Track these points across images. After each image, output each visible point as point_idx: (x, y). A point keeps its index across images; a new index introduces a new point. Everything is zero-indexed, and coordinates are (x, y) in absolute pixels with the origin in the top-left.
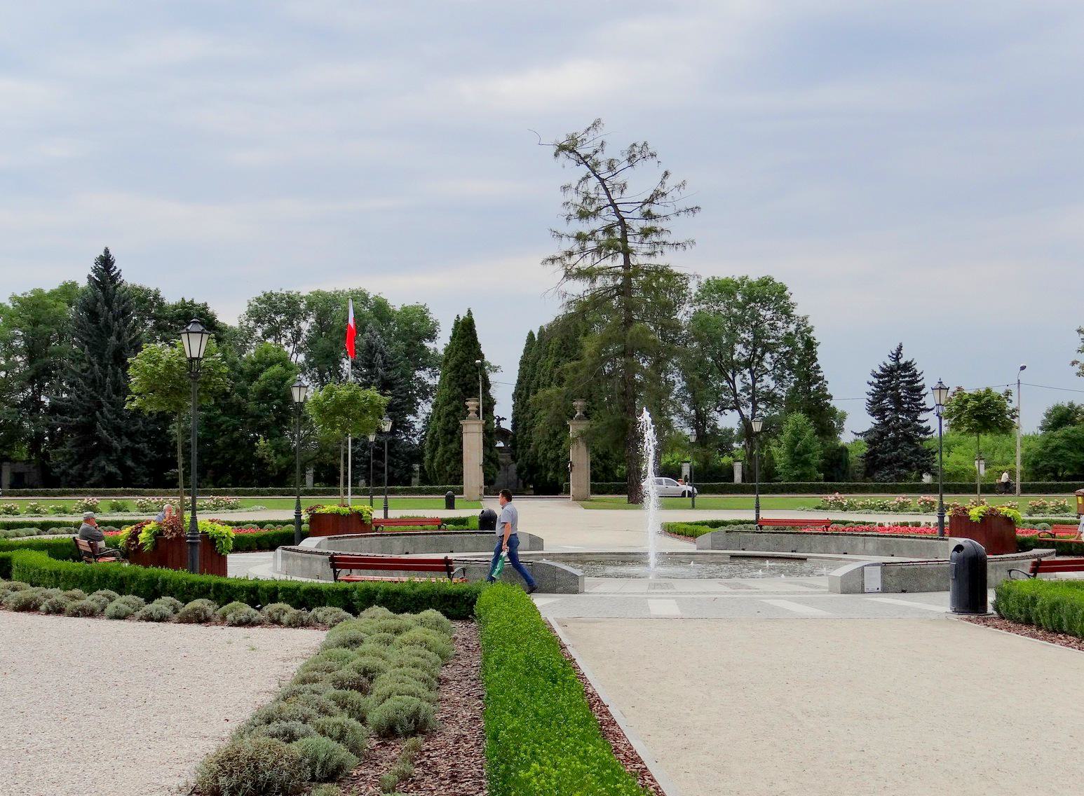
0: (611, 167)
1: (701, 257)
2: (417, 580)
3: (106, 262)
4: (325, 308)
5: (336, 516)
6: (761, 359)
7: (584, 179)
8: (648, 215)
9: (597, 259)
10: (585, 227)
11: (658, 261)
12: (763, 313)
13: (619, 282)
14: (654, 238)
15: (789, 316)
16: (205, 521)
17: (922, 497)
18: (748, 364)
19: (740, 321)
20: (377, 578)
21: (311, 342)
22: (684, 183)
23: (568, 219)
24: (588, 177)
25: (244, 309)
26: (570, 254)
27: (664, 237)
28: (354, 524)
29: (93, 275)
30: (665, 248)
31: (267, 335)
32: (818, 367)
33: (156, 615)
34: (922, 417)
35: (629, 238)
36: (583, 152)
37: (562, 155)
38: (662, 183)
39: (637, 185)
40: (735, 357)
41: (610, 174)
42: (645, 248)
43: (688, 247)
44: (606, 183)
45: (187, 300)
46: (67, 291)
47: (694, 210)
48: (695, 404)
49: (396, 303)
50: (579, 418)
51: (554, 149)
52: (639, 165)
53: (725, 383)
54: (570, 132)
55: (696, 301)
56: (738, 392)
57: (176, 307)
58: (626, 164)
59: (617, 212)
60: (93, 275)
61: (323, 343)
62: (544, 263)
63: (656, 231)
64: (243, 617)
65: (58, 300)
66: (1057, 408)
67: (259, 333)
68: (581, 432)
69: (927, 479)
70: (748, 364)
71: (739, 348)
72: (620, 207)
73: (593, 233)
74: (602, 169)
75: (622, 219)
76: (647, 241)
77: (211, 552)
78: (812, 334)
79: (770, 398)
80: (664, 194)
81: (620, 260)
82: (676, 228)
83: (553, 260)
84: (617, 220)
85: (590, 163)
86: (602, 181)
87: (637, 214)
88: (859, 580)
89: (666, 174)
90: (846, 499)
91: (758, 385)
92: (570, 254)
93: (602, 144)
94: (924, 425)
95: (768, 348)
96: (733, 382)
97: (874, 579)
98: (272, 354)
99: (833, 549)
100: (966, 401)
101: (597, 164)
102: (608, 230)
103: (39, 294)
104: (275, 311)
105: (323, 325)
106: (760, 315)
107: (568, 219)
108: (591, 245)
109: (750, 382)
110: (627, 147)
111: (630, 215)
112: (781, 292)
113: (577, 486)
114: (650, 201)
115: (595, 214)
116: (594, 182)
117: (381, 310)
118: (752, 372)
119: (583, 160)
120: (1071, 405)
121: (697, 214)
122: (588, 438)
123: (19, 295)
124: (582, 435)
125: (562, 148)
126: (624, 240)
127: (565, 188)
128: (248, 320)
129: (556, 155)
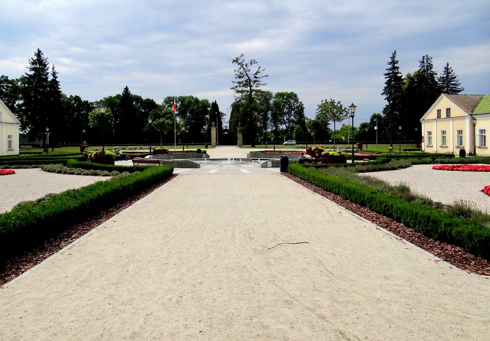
0: (246, 65)
1: (273, 87)
2: (149, 165)
3: (126, 89)
4: (182, 99)
5: (159, 150)
6: (291, 112)
7: (240, 68)
8: (255, 77)
9: (243, 88)
10: (241, 80)
11: (259, 88)
12: (291, 101)
13: (248, 93)
14: (257, 83)
15: (297, 101)
16: (107, 152)
17: (129, 147)
18: (287, 113)
19: (285, 103)
20: (143, 165)
21: (179, 109)
22: (264, 69)
23: (236, 78)
24: (241, 68)
25: (163, 101)
26: (237, 87)
27: (260, 83)
28: (164, 152)
29: (123, 93)
30: (260, 85)
31: (169, 107)
32: (304, 114)
33: (86, 174)
34: (328, 126)
35: (251, 83)
36: (239, 62)
37: (234, 63)
38: (259, 69)
39: (253, 70)
40: (284, 112)
41: (246, 67)
42: (255, 85)
43: (266, 85)
44: (245, 69)
45: (148, 98)
46: (118, 96)
47: (267, 76)
48: (275, 123)
49: (200, 99)
50: (214, 127)
51: (232, 61)
52: (253, 65)
53: (282, 118)
54: (237, 57)
55: (275, 98)
56: (285, 120)
57: (145, 100)
58: (250, 65)
59: (248, 77)
60: (123, 93)
61: (183, 109)
62: (231, 89)
63: (257, 81)
64: (104, 174)
65: (116, 99)
66: (363, 124)
67: (167, 106)
68: (240, 130)
69: (330, 141)
70: (287, 113)
71: (285, 109)
72: (249, 75)
73: (242, 82)
74: (244, 66)
75: (249, 78)
76: (255, 83)
77: (110, 159)
78: (303, 106)
79: (293, 121)
80: (259, 72)
81: (249, 88)
82: (263, 80)
83: (233, 88)
84: (248, 78)
85: (241, 64)
86: (244, 69)
87: (253, 77)
88: (266, 165)
89: (260, 67)
90: (143, 147)
91: (290, 118)
92: (237, 87)
93: (244, 60)
94: (328, 128)
95: (292, 109)
96: (284, 118)
97: (270, 164)
98: (168, 111)
99: (278, 157)
100: (311, 122)
101: (243, 65)
102: (246, 81)
103: (110, 97)
104: (169, 101)
105: (182, 105)
106: (290, 101)
107: (236, 78)
108: (242, 85)
109: (288, 117)
110: (250, 61)
111: (251, 77)
112: (295, 96)
113: (239, 143)
114: (256, 74)
115: (242, 77)
116: (242, 69)
117: (197, 100)
118: (288, 115)
119: (240, 64)
120: (366, 123)
121: (268, 77)
122: (242, 132)
123: (106, 98)
124: (240, 131)
125: (234, 61)
126: (250, 84)
127: (235, 71)
128: (164, 103)
129: (233, 63)
